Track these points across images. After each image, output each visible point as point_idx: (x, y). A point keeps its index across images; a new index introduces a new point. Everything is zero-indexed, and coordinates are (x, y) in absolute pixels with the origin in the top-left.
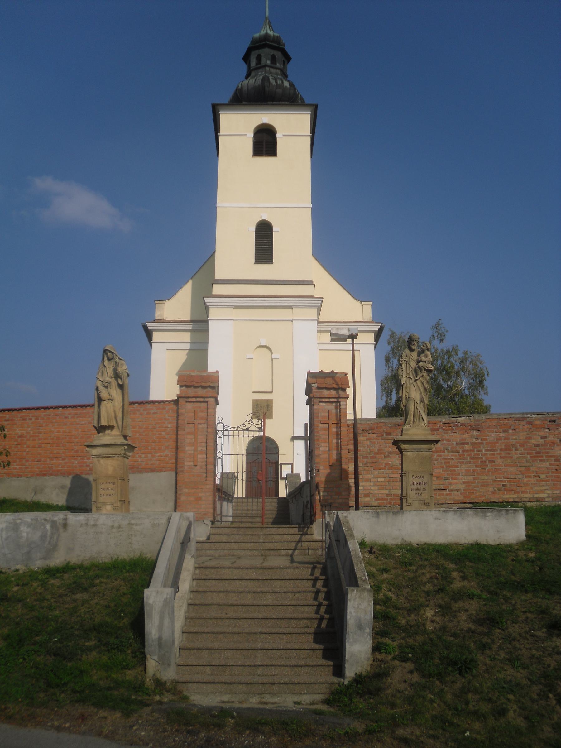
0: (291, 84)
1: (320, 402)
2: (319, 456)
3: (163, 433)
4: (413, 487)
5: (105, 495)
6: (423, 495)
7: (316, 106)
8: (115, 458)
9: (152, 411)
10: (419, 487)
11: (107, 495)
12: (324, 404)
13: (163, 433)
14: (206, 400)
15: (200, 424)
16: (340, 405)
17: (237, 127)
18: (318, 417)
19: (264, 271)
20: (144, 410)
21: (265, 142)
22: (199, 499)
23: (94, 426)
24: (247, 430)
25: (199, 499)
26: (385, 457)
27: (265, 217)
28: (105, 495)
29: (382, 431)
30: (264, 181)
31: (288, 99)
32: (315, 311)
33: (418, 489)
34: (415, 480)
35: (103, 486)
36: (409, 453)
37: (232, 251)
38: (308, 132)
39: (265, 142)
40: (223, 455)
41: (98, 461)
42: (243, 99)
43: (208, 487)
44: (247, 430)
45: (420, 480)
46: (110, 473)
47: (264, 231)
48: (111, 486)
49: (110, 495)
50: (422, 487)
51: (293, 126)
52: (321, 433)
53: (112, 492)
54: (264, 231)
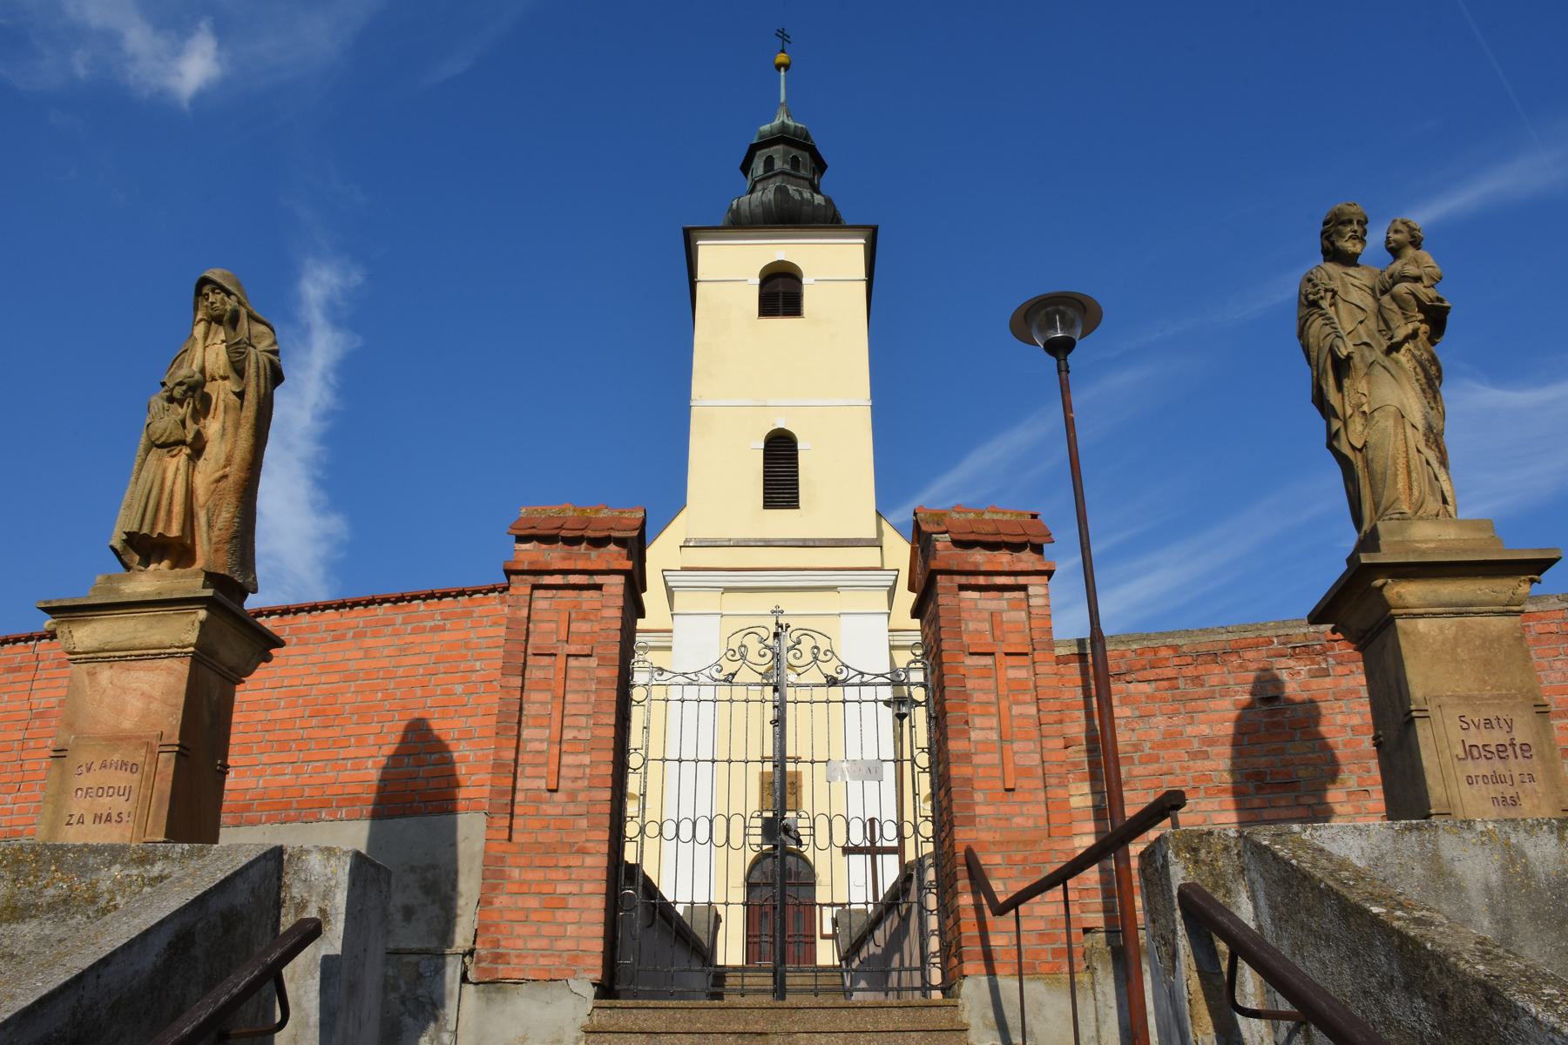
0: (828, 201)
1: (963, 588)
2: (966, 757)
3: (459, 689)
4: (1471, 768)
5: (88, 819)
6: (1526, 805)
7: (875, 230)
8: (158, 662)
9: (430, 624)
10: (1499, 766)
11: (98, 818)
12: (975, 595)
13: (459, 689)
14: (598, 579)
15: (577, 656)
16: (1028, 596)
17: (730, 267)
18: (959, 635)
19: (782, 522)
20: (405, 622)
21: (781, 293)
22: (556, 903)
23: (112, 548)
24: (729, 679)
25: (556, 903)
26: (1194, 755)
27: (781, 424)
28: (88, 819)
29: (1169, 673)
30: (782, 357)
31: (825, 221)
32: (884, 595)
33: (1497, 779)
34: (1476, 737)
35: (86, 780)
36: (1422, 624)
37: (721, 468)
38: (861, 273)
39: (781, 293)
40: (645, 760)
41: (92, 674)
42: (741, 224)
43: (589, 861)
44: (729, 679)
45: (1497, 737)
46: (127, 725)
47: (781, 453)
48: (123, 779)
49: (109, 819)
50: (1516, 766)
51: (832, 266)
52: (970, 684)
53: (119, 804)
54: (781, 453)
